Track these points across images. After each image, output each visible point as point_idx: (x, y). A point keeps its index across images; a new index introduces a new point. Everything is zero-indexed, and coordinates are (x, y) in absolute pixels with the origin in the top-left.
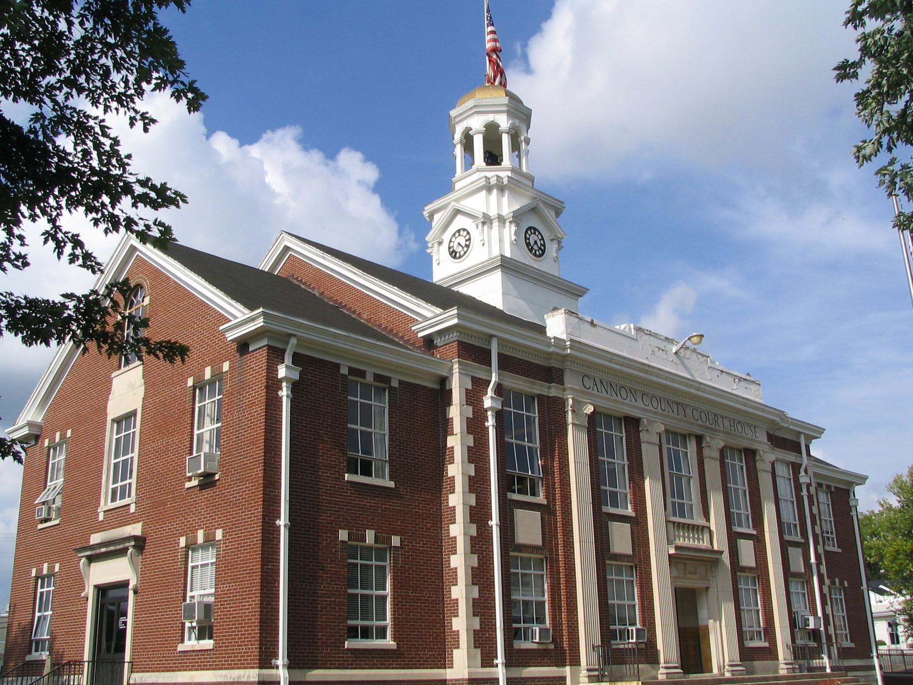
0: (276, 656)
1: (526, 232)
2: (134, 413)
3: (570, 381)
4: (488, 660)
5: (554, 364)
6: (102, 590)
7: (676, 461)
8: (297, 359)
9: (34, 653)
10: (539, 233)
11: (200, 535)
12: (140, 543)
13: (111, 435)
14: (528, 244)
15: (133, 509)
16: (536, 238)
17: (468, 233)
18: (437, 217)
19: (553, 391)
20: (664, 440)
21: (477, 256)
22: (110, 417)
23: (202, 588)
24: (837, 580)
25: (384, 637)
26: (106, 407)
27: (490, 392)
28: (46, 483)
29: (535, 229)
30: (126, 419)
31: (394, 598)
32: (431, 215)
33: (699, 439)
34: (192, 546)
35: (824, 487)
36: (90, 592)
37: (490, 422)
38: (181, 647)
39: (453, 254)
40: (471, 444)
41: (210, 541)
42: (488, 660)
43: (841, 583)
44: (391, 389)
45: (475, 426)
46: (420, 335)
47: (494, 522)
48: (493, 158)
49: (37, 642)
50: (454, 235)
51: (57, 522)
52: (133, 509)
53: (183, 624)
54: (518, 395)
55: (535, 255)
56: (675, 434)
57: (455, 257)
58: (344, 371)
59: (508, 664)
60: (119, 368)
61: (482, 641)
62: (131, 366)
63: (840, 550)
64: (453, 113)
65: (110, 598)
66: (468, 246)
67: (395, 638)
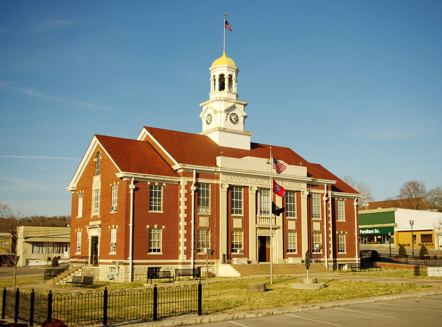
0: (129, 257)
4: (188, 258)
14: (231, 120)
15: (99, 217)
18: (204, 107)
21: (214, 125)
23: (114, 240)
25: (160, 251)
26: (92, 186)
31: (162, 242)
32: (202, 107)
34: (111, 228)
37: (193, 194)
39: (208, 123)
40: (186, 200)
41: (115, 227)
42: (188, 258)
45: (188, 195)
47: (192, 221)
48: (222, 87)
60: (95, 175)
61: (188, 253)
64: (210, 69)
65: (95, 239)
66: (211, 121)
67: (162, 252)
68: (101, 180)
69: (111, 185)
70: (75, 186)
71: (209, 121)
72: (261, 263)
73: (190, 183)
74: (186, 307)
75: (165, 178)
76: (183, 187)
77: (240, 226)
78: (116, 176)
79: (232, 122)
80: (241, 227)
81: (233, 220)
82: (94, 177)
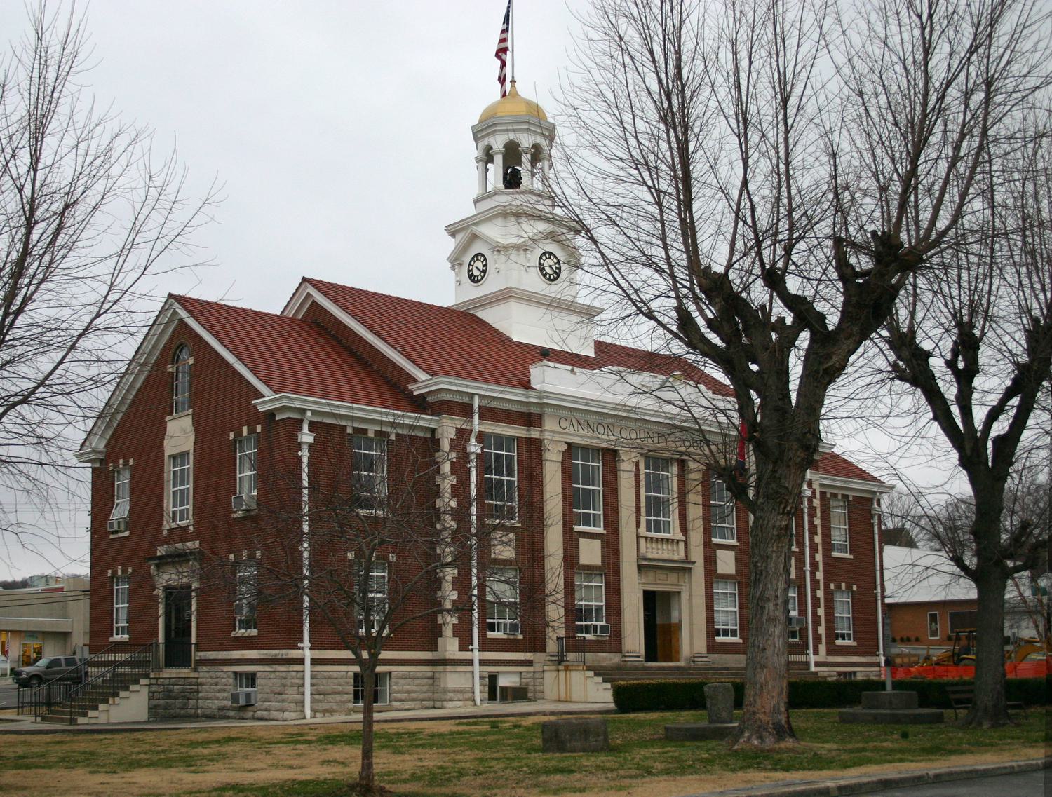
0: (302, 641)
1: (541, 258)
2: (187, 453)
3: (549, 424)
5: (534, 410)
6: (169, 590)
7: (655, 484)
8: (313, 426)
9: (115, 636)
10: (555, 257)
11: (245, 553)
12: (199, 556)
13: (169, 469)
14: (542, 270)
16: (551, 263)
17: (485, 259)
19: (534, 434)
20: (642, 466)
22: (167, 453)
24: (843, 585)
27: (473, 440)
28: (113, 501)
29: (550, 253)
30: (179, 458)
33: (682, 465)
35: (840, 497)
36: (159, 592)
38: (233, 634)
43: (849, 588)
44: (390, 442)
46: (415, 393)
49: (117, 628)
50: (473, 259)
51: (127, 533)
52: (191, 528)
53: (235, 619)
54: (499, 438)
55: (549, 279)
56: (656, 459)
57: (473, 281)
58: (349, 431)
59: (482, 649)
60: (171, 413)
62: (180, 414)
63: (851, 557)
66: (484, 272)
68: (195, 423)
69: (232, 435)
70: (102, 446)
71: (476, 273)
72: (649, 664)
73: (463, 434)
74: (35, 694)
75: (501, 392)
76: (445, 445)
77: (597, 561)
78: (255, 407)
79: (545, 276)
80: (599, 563)
81: (577, 544)
82: (168, 418)
